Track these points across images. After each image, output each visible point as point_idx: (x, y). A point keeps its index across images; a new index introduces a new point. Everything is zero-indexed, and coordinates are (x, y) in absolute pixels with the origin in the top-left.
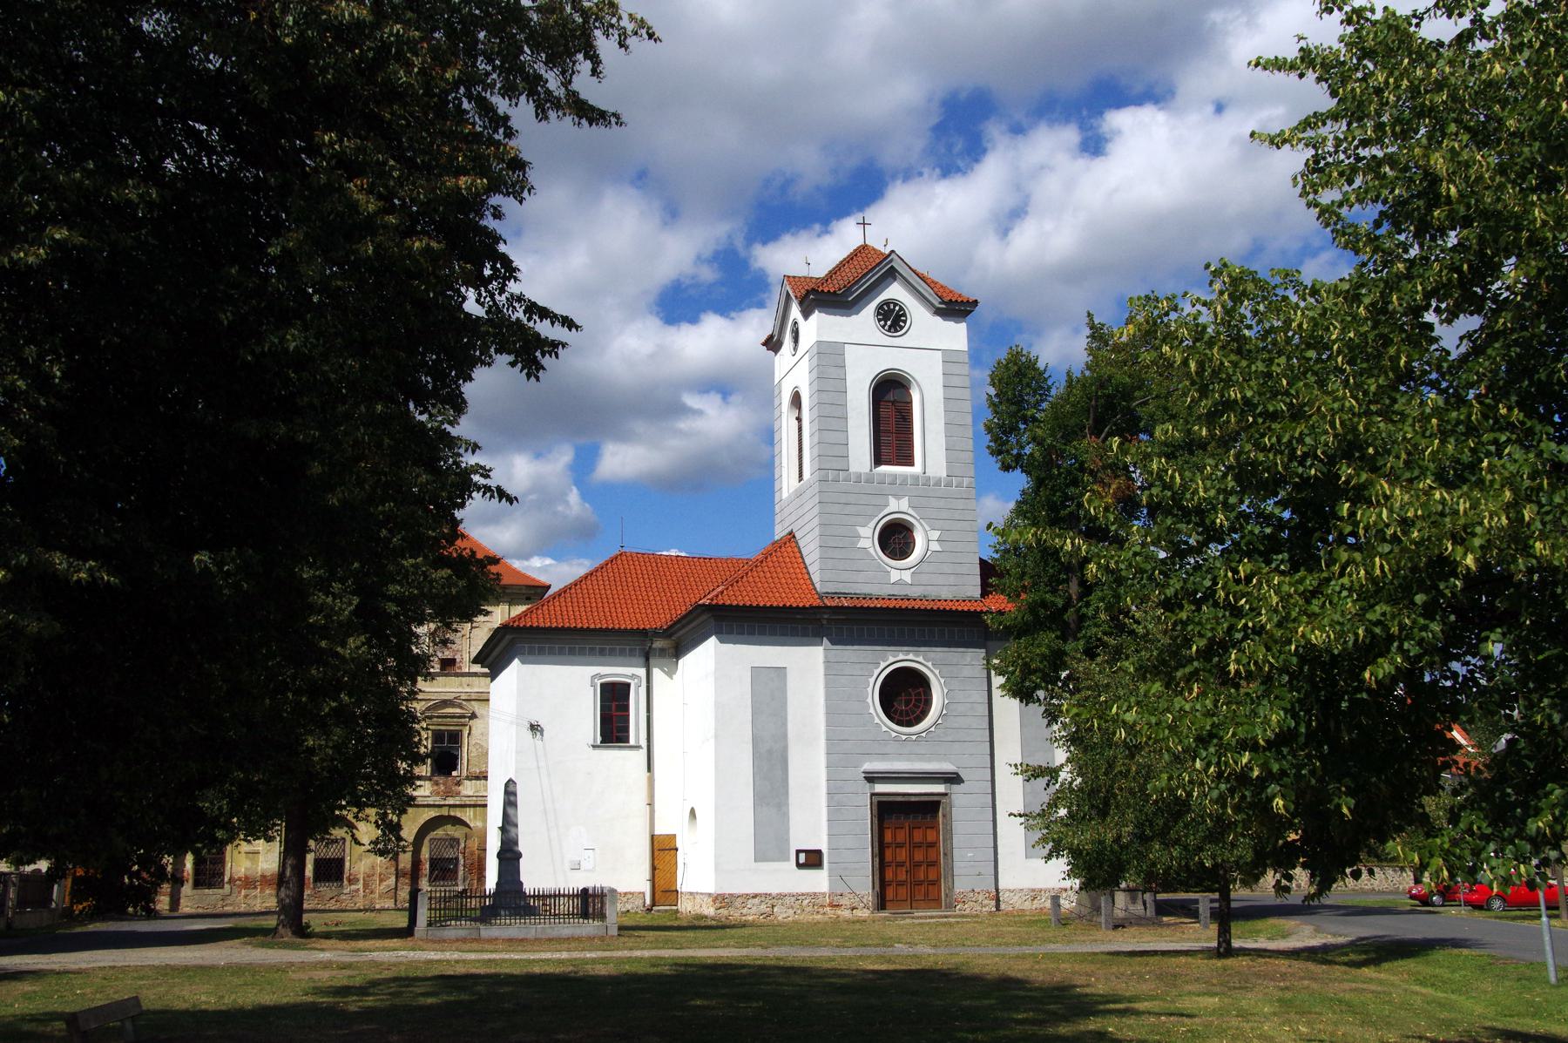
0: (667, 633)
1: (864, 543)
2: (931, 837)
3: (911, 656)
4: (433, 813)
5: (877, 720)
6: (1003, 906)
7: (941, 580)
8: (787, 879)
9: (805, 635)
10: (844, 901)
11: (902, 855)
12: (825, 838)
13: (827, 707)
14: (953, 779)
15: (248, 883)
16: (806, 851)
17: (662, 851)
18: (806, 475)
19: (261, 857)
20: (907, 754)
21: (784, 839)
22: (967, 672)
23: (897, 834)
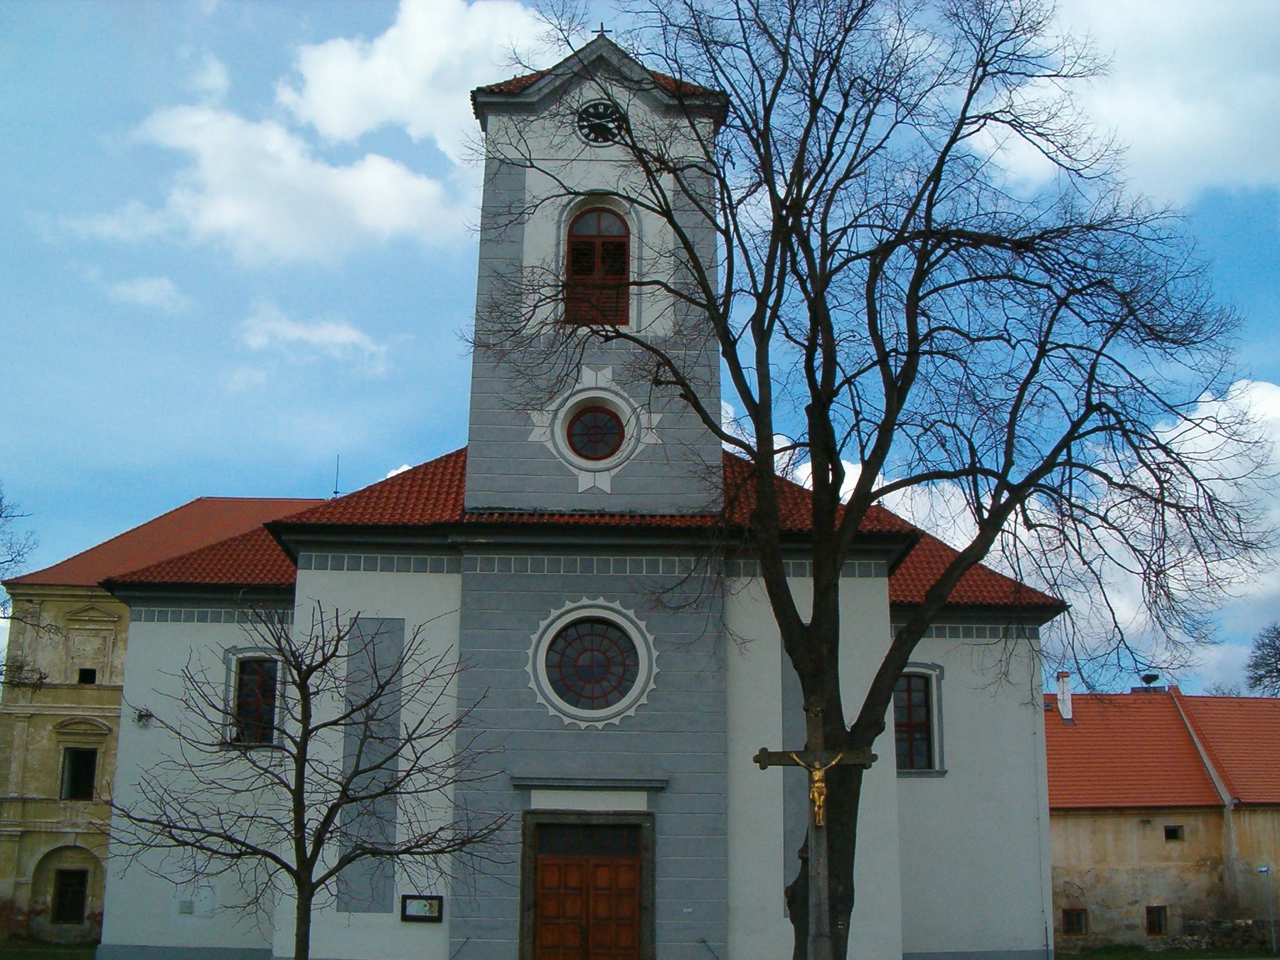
1: (588, 377)
3: (601, 601)
14: (656, 788)
20: (585, 761)
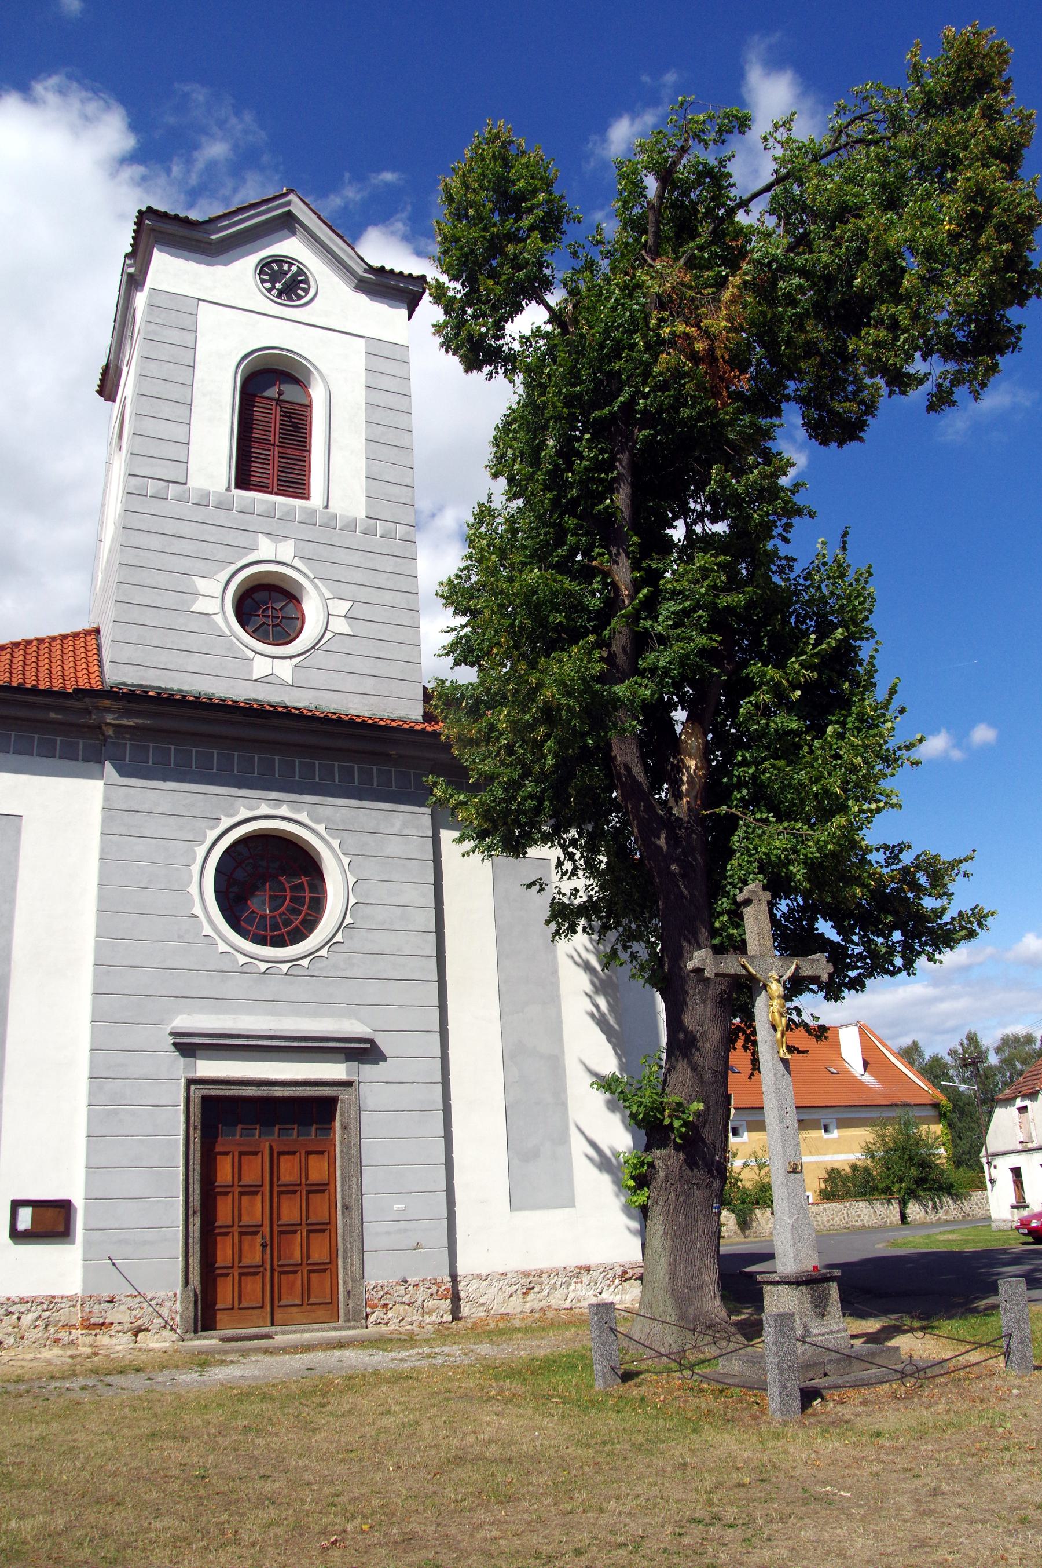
1: (200, 605)
2: (317, 1170)
3: (284, 811)
5: (207, 930)
6: (465, 1310)
7: (350, 683)
9: (69, 755)
10: (118, 1315)
11: (255, 1210)
13: (101, 898)
14: (364, 1052)
16: (37, 1205)
20: (267, 1000)
22: (394, 847)
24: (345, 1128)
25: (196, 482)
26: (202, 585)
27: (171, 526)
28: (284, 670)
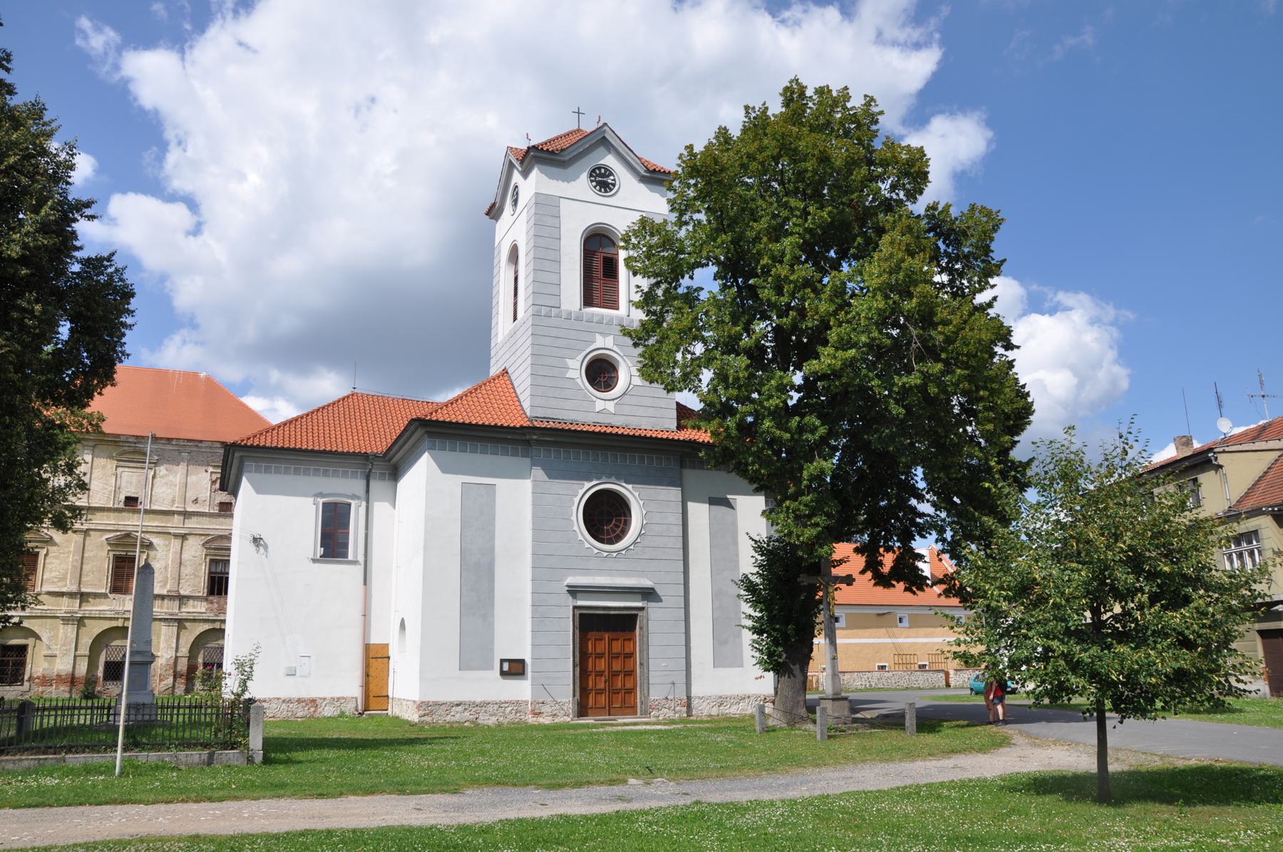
0: (387, 456)
1: (570, 374)
4: (207, 627)
5: (580, 537)
7: (641, 412)
8: (492, 688)
10: (546, 709)
11: (602, 665)
12: (529, 647)
14: (648, 594)
15: (45, 681)
16: (510, 661)
17: (375, 660)
18: (520, 316)
19: (58, 660)
20: (608, 570)
21: (488, 647)
23: (601, 643)
24: (641, 628)
25: (565, 306)
26: (571, 363)
27: (554, 332)
28: (610, 406)
